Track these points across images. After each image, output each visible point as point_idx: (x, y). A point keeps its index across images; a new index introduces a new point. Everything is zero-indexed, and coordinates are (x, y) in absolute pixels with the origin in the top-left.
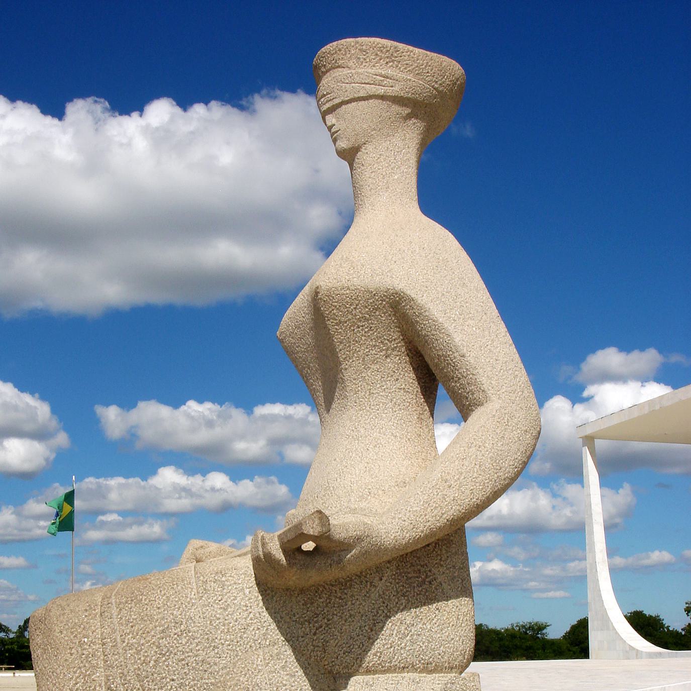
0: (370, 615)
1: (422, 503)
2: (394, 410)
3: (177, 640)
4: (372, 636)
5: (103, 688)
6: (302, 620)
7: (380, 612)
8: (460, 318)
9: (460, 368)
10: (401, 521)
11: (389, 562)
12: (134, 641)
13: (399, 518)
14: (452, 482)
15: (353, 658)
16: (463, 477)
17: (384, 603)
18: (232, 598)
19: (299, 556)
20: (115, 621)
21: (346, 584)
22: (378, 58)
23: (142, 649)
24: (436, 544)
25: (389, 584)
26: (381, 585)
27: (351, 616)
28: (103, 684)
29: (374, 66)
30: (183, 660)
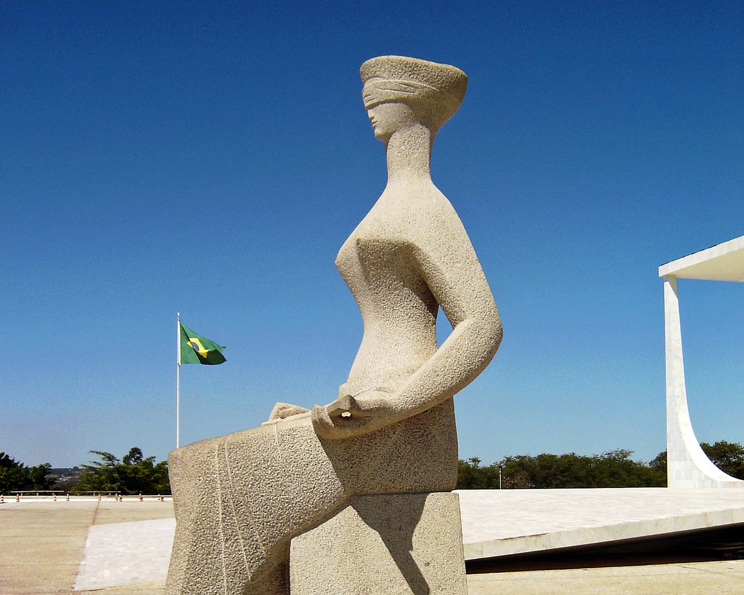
0: (387, 456)
1: (419, 386)
2: (409, 321)
3: (266, 472)
4: (388, 469)
5: (220, 501)
6: (343, 459)
7: (394, 454)
8: (450, 262)
9: (450, 296)
10: (405, 397)
11: (400, 422)
12: (239, 472)
13: (404, 396)
14: (439, 373)
15: (376, 483)
16: (446, 369)
17: (396, 448)
18: (300, 445)
19: (340, 421)
20: (227, 459)
21: (372, 436)
22: (404, 72)
23: (243, 477)
24: (432, 410)
25: (399, 436)
26: (394, 437)
27: (375, 456)
28: (219, 498)
29: (401, 77)
30: (269, 484)
